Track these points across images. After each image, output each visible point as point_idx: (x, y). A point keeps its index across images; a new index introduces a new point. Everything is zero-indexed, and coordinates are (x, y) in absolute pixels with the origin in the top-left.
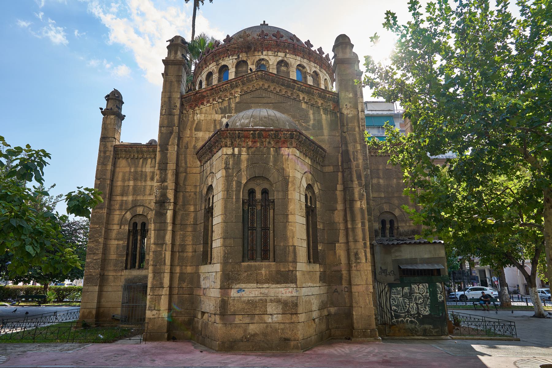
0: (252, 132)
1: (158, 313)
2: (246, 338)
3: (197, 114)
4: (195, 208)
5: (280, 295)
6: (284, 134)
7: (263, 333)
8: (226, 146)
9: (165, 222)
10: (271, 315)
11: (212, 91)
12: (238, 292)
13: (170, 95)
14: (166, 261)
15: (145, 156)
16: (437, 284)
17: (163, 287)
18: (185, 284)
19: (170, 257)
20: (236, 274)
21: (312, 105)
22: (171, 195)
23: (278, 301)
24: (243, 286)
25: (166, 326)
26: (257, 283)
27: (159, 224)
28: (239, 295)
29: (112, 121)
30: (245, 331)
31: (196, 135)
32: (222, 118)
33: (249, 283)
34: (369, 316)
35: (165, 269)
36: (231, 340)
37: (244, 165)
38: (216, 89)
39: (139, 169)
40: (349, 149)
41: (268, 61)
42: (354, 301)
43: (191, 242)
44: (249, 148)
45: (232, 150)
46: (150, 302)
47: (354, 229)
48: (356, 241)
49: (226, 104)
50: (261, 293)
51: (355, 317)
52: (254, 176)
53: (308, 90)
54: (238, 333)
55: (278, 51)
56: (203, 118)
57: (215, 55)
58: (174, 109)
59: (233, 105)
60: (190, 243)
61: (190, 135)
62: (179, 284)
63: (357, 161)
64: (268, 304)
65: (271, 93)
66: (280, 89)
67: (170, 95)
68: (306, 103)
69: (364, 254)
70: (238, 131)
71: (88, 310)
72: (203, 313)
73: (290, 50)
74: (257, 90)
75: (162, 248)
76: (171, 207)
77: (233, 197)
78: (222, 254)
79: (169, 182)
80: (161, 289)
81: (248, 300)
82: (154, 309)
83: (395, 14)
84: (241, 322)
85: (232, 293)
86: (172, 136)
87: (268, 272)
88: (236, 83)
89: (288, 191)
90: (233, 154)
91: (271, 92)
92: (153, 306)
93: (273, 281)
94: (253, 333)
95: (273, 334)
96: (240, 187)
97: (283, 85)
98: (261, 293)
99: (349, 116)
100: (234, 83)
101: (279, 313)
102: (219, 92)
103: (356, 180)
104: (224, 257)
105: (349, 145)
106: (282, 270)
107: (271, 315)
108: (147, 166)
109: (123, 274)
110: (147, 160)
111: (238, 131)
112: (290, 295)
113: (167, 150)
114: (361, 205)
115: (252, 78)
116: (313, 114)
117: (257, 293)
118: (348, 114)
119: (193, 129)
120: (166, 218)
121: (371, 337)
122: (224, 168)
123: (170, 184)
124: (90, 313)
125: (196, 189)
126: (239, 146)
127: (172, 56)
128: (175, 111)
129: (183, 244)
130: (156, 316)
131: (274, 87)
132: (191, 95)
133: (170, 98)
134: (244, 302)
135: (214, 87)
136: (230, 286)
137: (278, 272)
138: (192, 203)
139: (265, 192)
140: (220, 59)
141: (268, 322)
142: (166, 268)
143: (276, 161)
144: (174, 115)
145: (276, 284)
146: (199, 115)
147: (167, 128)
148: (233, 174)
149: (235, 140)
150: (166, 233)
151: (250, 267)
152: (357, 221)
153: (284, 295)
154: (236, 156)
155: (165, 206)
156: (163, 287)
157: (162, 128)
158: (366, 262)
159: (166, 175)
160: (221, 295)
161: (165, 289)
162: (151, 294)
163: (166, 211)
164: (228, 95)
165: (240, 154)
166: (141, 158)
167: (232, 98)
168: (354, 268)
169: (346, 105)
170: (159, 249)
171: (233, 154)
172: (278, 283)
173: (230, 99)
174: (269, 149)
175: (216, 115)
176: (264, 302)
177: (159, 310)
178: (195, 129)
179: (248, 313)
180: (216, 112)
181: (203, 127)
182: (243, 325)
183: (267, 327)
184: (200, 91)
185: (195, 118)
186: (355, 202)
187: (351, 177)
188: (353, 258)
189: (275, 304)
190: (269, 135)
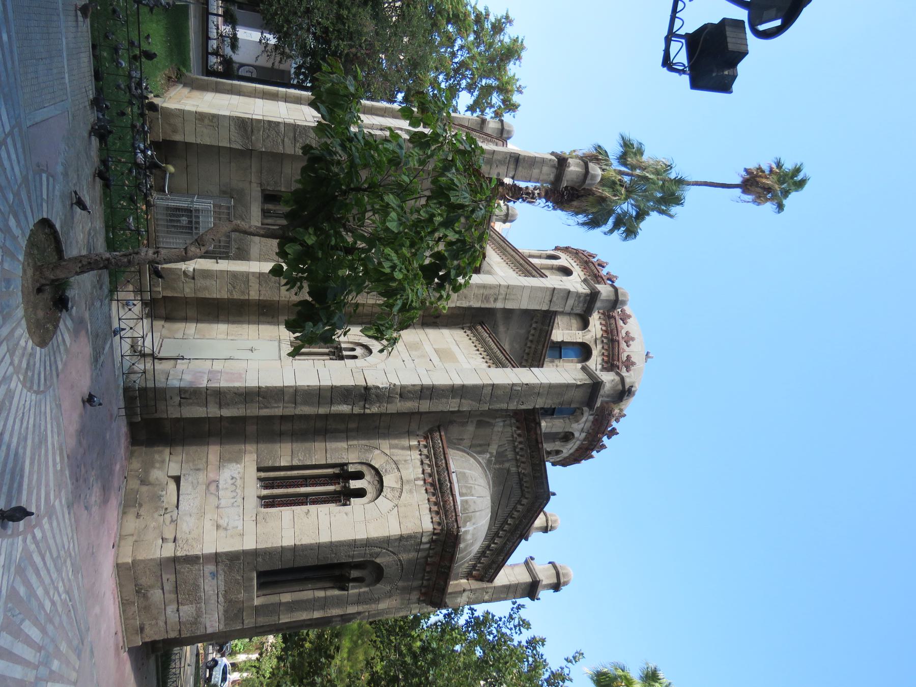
3: (504, 421)
10: (178, 610)
12: (211, 573)
17: (220, 408)
20: (240, 568)
23: (199, 615)
24: (221, 577)
30: (151, 587)
76: (357, 410)
83: (669, 167)
85: (209, 567)
94: (149, 595)
101: (181, 618)
109: (254, 185)
112: (208, 625)
114: (336, 621)
128: (515, 403)
156: (220, 408)
176: (197, 600)
180: (501, 445)
185: (497, 420)
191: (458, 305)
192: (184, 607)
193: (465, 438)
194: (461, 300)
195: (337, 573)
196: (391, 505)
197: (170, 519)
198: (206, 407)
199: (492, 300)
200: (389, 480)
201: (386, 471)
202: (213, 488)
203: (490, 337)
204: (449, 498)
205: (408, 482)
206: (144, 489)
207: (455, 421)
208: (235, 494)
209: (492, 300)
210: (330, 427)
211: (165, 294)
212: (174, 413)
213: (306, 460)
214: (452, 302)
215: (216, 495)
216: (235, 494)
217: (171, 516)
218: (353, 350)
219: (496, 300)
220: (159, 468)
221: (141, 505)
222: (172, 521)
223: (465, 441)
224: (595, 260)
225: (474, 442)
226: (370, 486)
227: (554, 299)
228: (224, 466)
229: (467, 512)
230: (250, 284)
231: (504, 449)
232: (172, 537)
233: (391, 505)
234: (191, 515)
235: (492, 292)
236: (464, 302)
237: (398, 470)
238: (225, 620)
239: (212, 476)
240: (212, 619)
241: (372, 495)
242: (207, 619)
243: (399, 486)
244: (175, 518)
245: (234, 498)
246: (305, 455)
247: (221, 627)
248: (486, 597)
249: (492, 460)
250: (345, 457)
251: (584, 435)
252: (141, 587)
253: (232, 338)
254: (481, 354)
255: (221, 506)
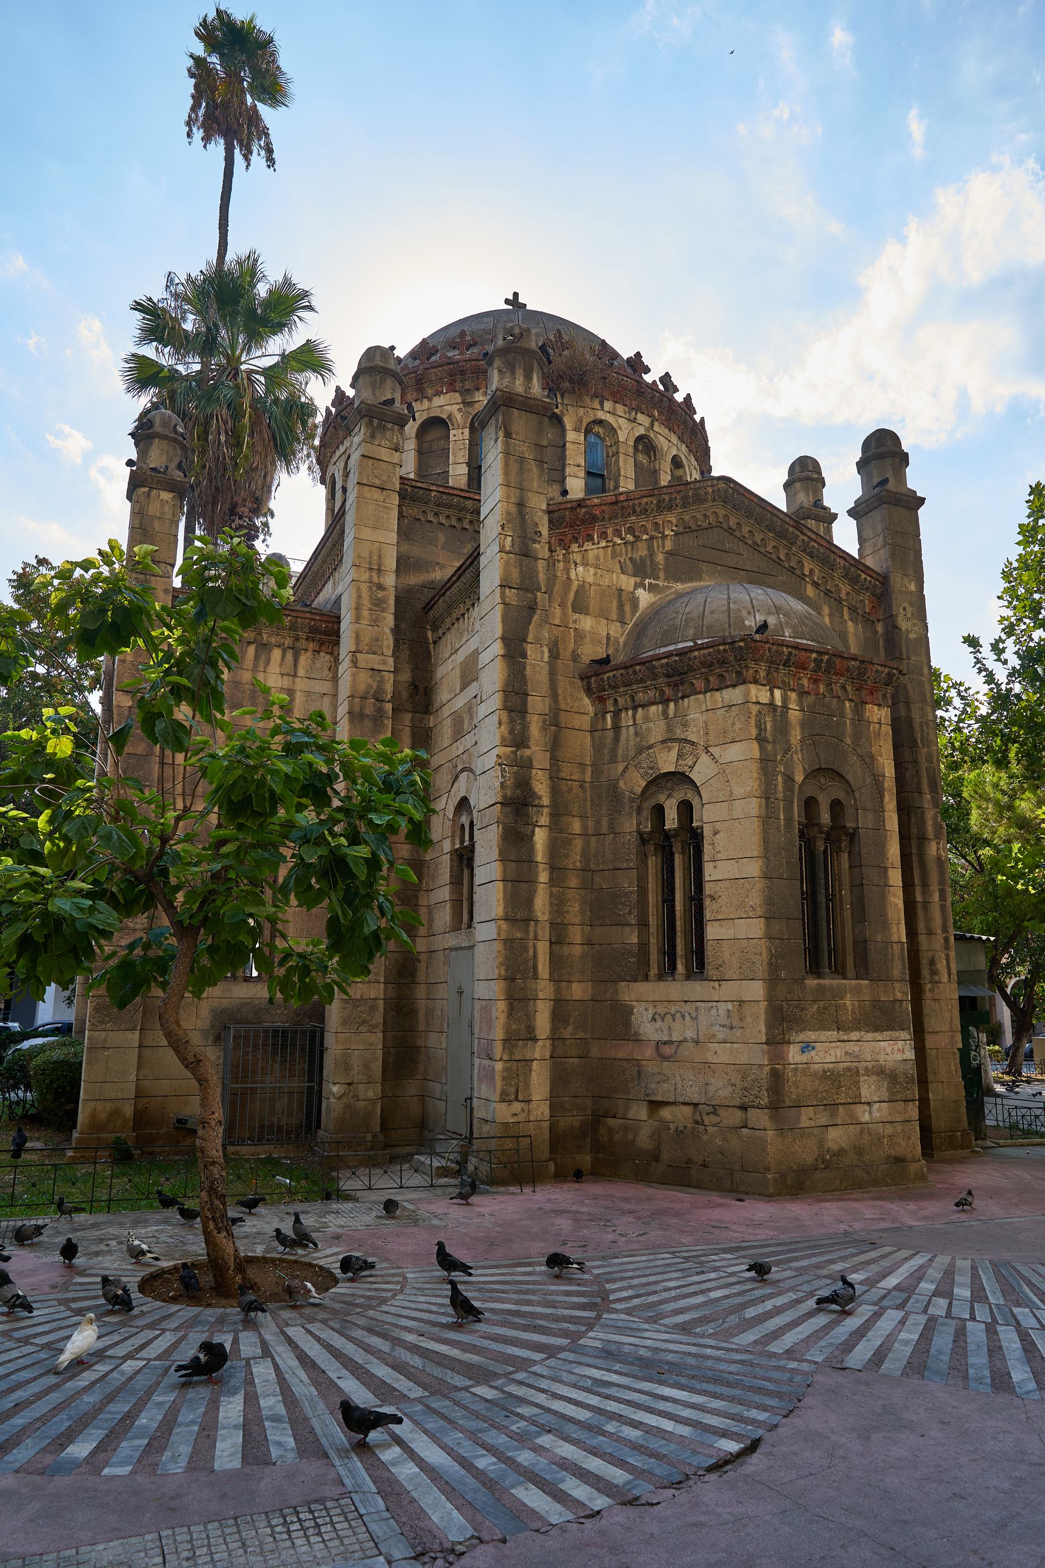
0: (814, 655)
1: (526, 1108)
2: (823, 1161)
3: (576, 564)
4: (584, 827)
5: (882, 1058)
6: (877, 671)
7: (855, 1147)
8: (756, 682)
9: (531, 861)
10: (869, 1103)
11: (616, 507)
13: (522, 496)
14: (540, 967)
15: (265, 636)
16: (971, 1028)
17: (535, 1040)
18: (570, 1029)
19: (548, 957)
20: (797, 1007)
21: (828, 593)
22: (541, 786)
23: (880, 1071)
24: (811, 1035)
25: (547, 1143)
26: (839, 1029)
27: (513, 864)
28: (804, 1058)
29: (166, 509)
30: (821, 1144)
31: (575, 621)
32: (637, 586)
33: (823, 1028)
34: (956, 1102)
35: (536, 990)
36: (795, 1168)
37: (796, 736)
38: (625, 504)
39: (246, 676)
40: (913, 716)
41: (613, 429)
42: (929, 1069)
43: (579, 917)
44: (802, 694)
45: (768, 694)
46: (504, 1079)
47: (926, 904)
48: (930, 933)
49: (642, 551)
50: (846, 1053)
51: (932, 1104)
52: (817, 767)
53: (824, 554)
54: (806, 1151)
55: (638, 410)
56: (590, 579)
57: (463, 373)
58: (534, 541)
59: (660, 558)
60: (577, 921)
61: (561, 620)
62: (554, 1029)
63: (928, 747)
64: (862, 1079)
65: (741, 543)
66: (762, 536)
67: (522, 496)
68: (816, 585)
69: (945, 962)
70: (787, 646)
71: (109, 1106)
72: (655, 1105)
73: (660, 413)
74: (711, 527)
75: (527, 932)
76: (544, 820)
77: (779, 814)
78: (764, 957)
79: (534, 748)
80: (530, 1043)
81: (824, 1072)
82: (517, 1099)
84: (812, 1123)
85: (791, 1055)
86: (536, 618)
87: (856, 1004)
88: (671, 500)
89: (883, 811)
90: (772, 704)
91: (742, 539)
92: (513, 1089)
93: (868, 1026)
94: (836, 1148)
95: (873, 1148)
96: (793, 792)
97: (770, 528)
98: (846, 1053)
99: (911, 636)
100: (667, 498)
101: (883, 1098)
102: (629, 515)
103: (927, 791)
104: (770, 964)
105: (912, 707)
106: (883, 998)
107: (869, 1103)
108: (270, 669)
110: (271, 650)
111: (787, 646)
112: (899, 1057)
113: (524, 655)
114: (938, 849)
115: (706, 493)
116: (831, 615)
117: (839, 1053)
118: (908, 632)
119: (569, 604)
120: (531, 850)
121: (962, 1147)
122: (756, 738)
123: (537, 752)
124: (116, 1113)
125: (583, 772)
126: (785, 687)
127: (518, 382)
128: (537, 546)
129: (559, 920)
130: (521, 1118)
131: (749, 529)
132: (566, 509)
133: (521, 505)
134: (816, 1074)
135: (622, 498)
136: (787, 1038)
137: (876, 1003)
138: (575, 810)
139: (837, 806)
140: (478, 389)
141: (863, 1120)
142: (539, 988)
143: (857, 735)
144: (536, 559)
145: (873, 1032)
146: (580, 569)
147: (521, 592)
148: (776, 755)
149: (777, 670)
150: (535, 891)
151: (821, 989)
152: (932, 888)
153: (890, 1058)
154: (779, 709)
155: (528, 815)
156: (535, 1040)
157: (507, 590)
158: (949, 981)
159: (525, 727)
160: (770, 1060)
161: (540, 1043)
162: (505, 1057)
163: (530, 827)
164: (649, 526)
165: (785, 707)
166: (249, 643)
167: (657, 538)
168: (928, 995)
169: (904, 609)
170: (519, 935)
171: (772, 704)
172: (877, 1029)
173: (652, 538)
174: (841, 702)
175: (623, 576)
176: (854, 1074)
177: (529, 1101)
178: (573, 605)
179: (825, 1102)
180: (621, 567)
181: (593, 604)
182: (816, 1131)
183: (862, 1131)
184: (588, 502)
185: (573, 576)
186: (926, 842)
187: (919, 784)
188: (925, 972)
189: (875, 1078)
190: (848, 670)
191: (390, 653)
192: (863, 1094)
193: (605, 634)
194: (381, 647)
195: (820, 846)
196: (704, 758)
197: (712, 1116)
198: (532, 1061)
199: (381, 594)
200: (667, 762)
201: (650, 768)
202: (667, 1050)
203: (444, 594)
204: (695, 657)
205: (670, 729)
206: (665, 1156)
207: (574, 651)
208: (678, 1016)
209: (381, 594)
210: (578, 864)
211: (378, 1129)
212: (541, 1110)
213: (630, 902)
214: (385, 663)
215: (678, 1046)
216: (678, 1016)
217: (708, 1114)
218: (463, 826)
219: (381, 587)
220: (636, 1134)
221: (689, 1161)
222: (715, 1113)
223: (612, 633)
224: (333, 410)
225: (615, 618)
226: (675, 794)
227: (377, 482)
228: (637, 1034)
229: (726, 625)
230: (359, 997)
231: (628, 562)
232: (739, 1113)
233: (704, 758)
234: (707, 1084)
235: (365, 594)
236: (385, 643)
237: (650, 747)
238: (893, 1029)
239: (649, 1052)
240: (889, 1050)
241: (689, 791)
242: (889, 1058)
243: (676, 746)
244: (710, 1109)
245: (683, 1017)
246: (623, 904)
247: (905, 1035)
248: (913, 587)
249: (650, 584)
250: (628, 837)
251: (641, 418)
252: (820, 1161)
253: (446, 1024)
254: (468, 610)
255: (695, 1037)
